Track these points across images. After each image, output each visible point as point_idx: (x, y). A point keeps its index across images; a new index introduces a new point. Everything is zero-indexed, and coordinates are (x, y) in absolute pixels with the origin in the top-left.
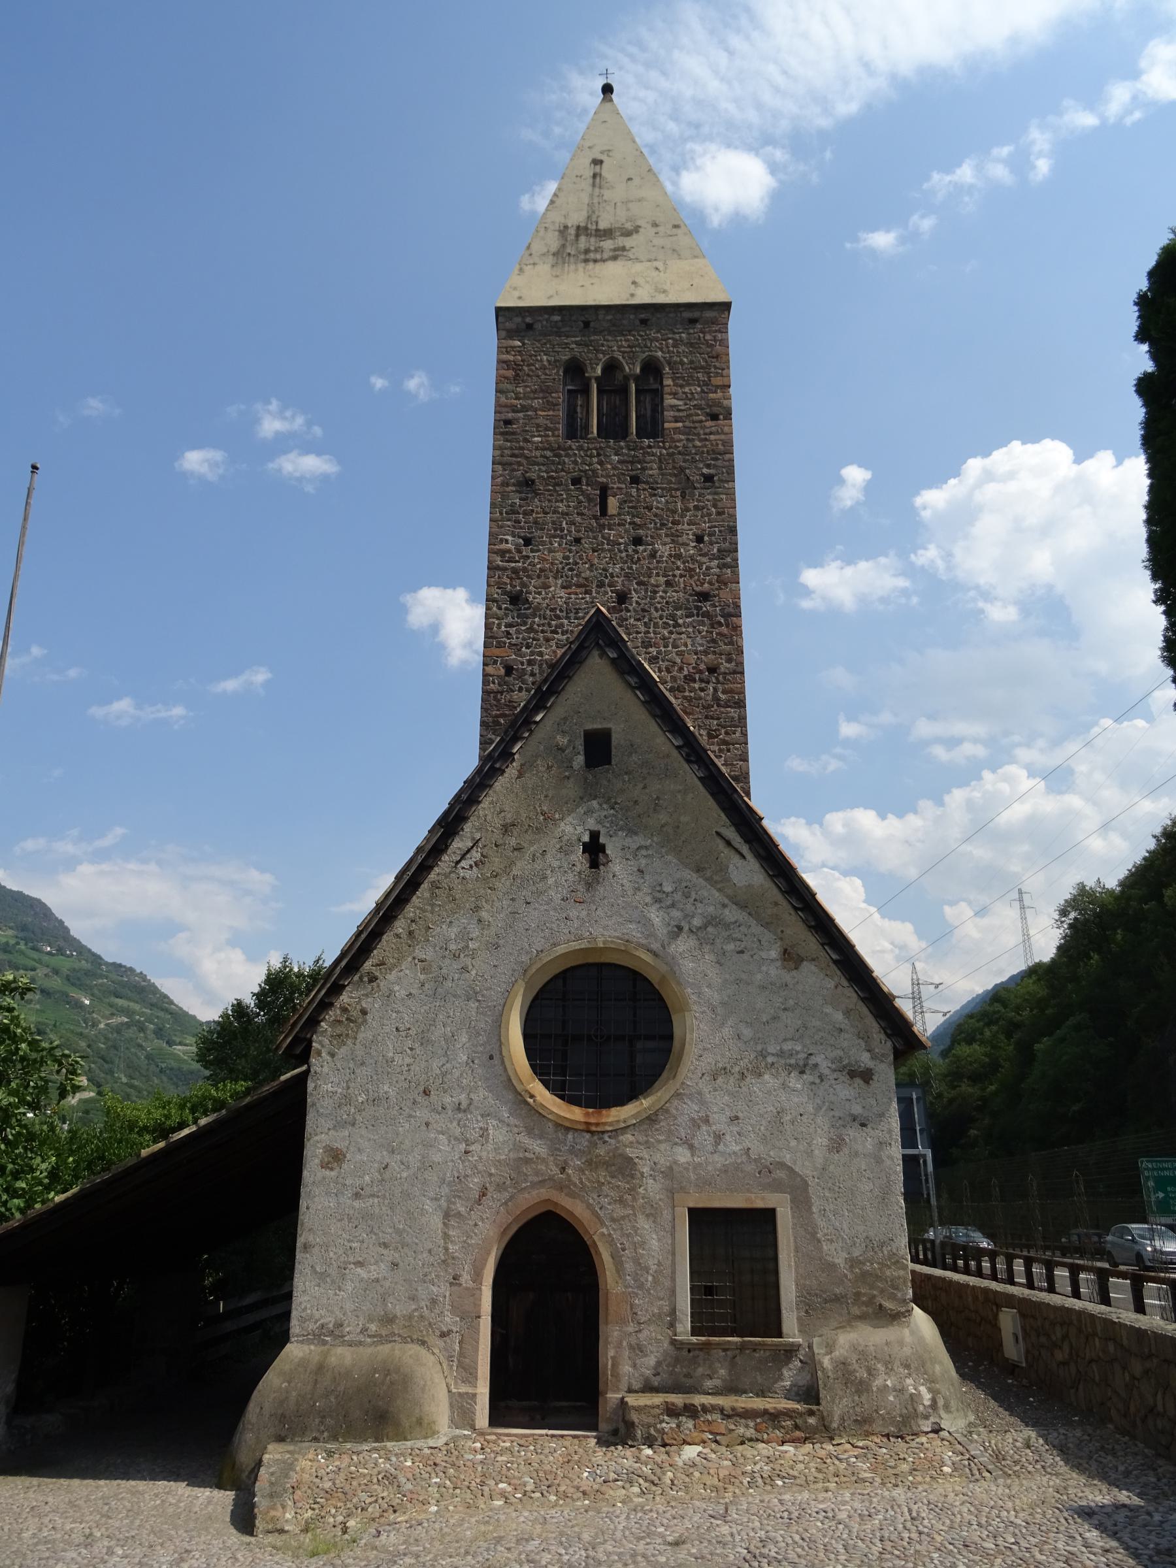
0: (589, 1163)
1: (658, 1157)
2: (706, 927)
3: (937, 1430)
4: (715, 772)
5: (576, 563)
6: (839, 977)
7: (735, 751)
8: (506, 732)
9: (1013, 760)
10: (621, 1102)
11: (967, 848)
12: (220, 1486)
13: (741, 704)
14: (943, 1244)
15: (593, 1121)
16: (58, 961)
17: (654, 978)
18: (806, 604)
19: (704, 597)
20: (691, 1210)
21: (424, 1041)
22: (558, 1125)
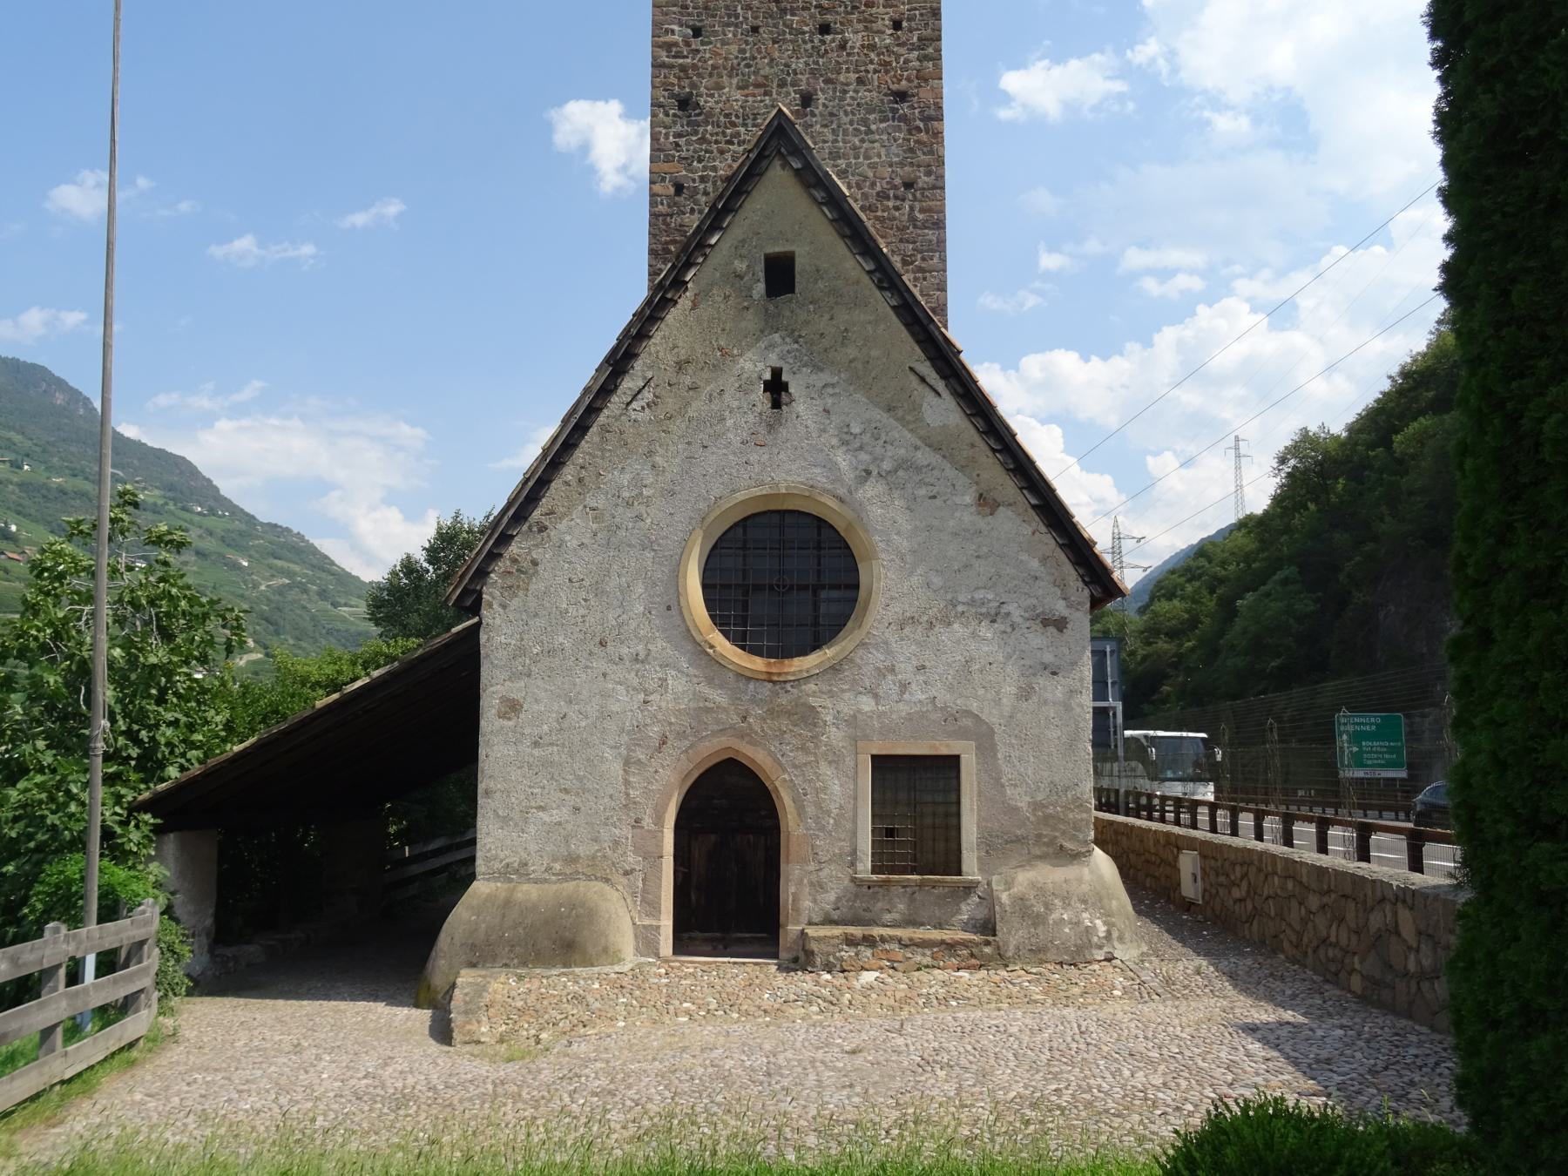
0: (771, 712)
1: (841, 706)
2: (896, 471)
3: (1110, 959)
4: (910, 300)
5: (754, 58)
6: (1037, 523)
7: (932, 279)
8: (678, 257)
9: (1231, 293)
10: (804, 652)
11: (1177, 392)
12: (417, 1006)
13: (939, 225)
14: (1127, 793)
15: (774, 670)
16: (210, 522)
17: (840, 526)
18: (1004, 114)
19: (901, 96)
20: (873, 757)
21: (598, 590)
22: (739, 676)
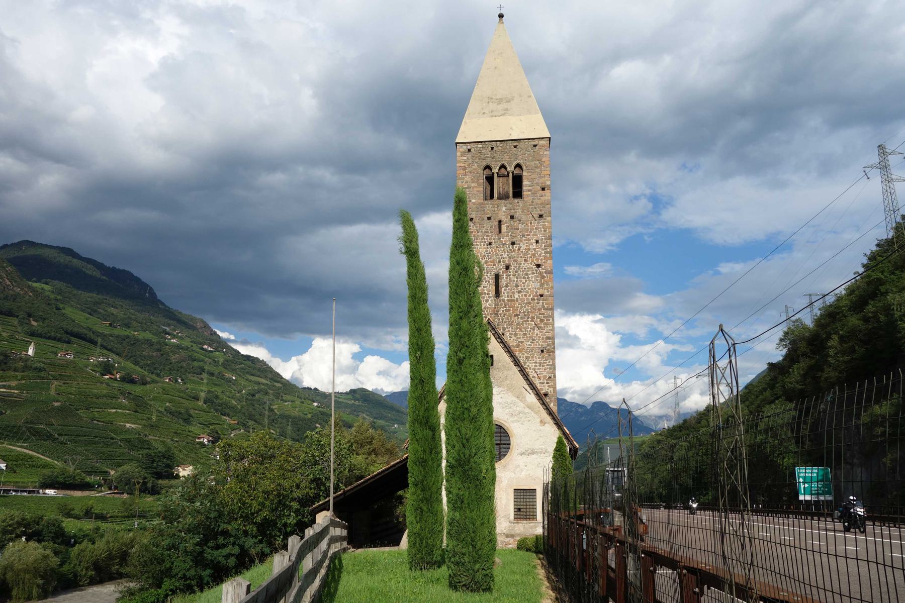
6: (555, 427)
